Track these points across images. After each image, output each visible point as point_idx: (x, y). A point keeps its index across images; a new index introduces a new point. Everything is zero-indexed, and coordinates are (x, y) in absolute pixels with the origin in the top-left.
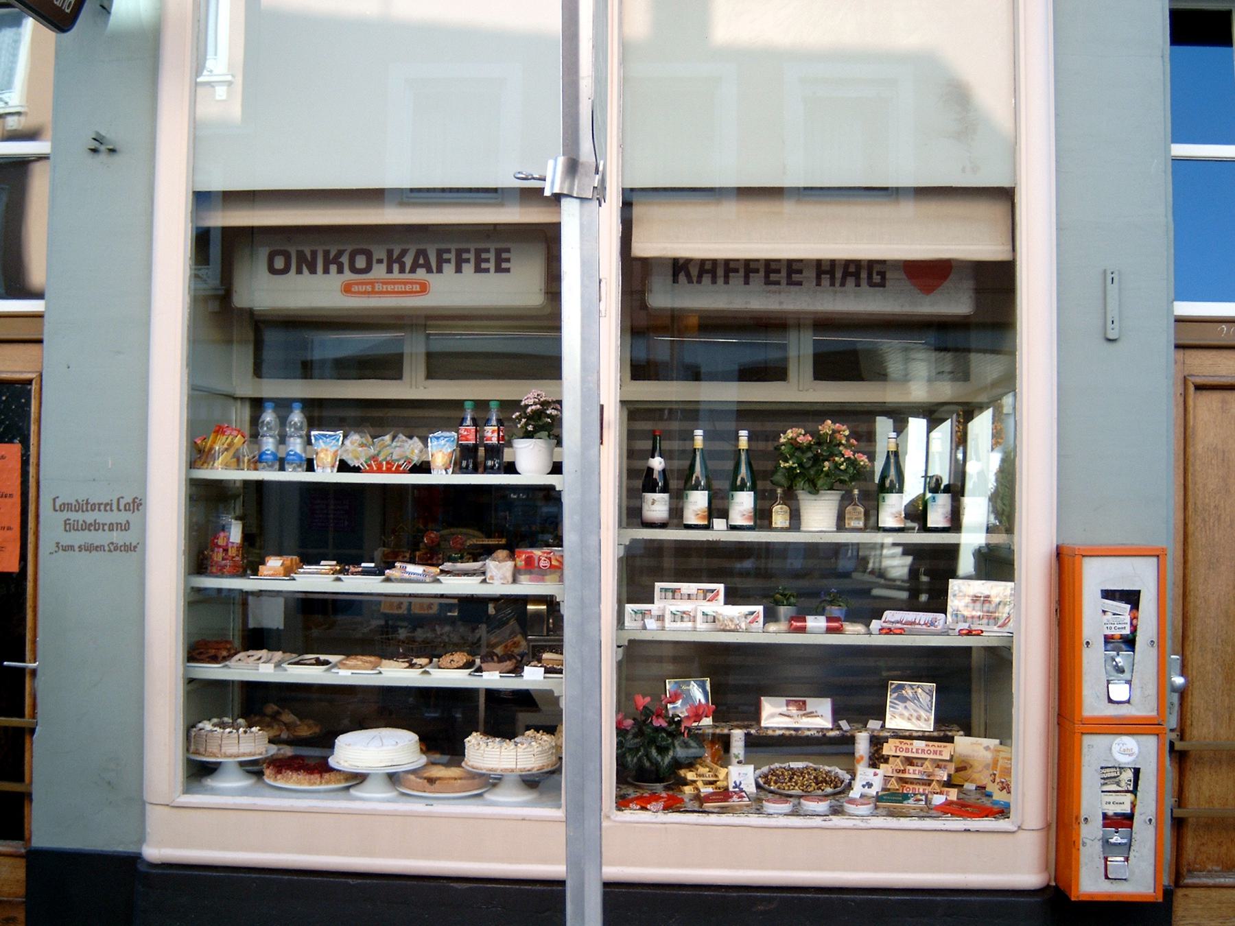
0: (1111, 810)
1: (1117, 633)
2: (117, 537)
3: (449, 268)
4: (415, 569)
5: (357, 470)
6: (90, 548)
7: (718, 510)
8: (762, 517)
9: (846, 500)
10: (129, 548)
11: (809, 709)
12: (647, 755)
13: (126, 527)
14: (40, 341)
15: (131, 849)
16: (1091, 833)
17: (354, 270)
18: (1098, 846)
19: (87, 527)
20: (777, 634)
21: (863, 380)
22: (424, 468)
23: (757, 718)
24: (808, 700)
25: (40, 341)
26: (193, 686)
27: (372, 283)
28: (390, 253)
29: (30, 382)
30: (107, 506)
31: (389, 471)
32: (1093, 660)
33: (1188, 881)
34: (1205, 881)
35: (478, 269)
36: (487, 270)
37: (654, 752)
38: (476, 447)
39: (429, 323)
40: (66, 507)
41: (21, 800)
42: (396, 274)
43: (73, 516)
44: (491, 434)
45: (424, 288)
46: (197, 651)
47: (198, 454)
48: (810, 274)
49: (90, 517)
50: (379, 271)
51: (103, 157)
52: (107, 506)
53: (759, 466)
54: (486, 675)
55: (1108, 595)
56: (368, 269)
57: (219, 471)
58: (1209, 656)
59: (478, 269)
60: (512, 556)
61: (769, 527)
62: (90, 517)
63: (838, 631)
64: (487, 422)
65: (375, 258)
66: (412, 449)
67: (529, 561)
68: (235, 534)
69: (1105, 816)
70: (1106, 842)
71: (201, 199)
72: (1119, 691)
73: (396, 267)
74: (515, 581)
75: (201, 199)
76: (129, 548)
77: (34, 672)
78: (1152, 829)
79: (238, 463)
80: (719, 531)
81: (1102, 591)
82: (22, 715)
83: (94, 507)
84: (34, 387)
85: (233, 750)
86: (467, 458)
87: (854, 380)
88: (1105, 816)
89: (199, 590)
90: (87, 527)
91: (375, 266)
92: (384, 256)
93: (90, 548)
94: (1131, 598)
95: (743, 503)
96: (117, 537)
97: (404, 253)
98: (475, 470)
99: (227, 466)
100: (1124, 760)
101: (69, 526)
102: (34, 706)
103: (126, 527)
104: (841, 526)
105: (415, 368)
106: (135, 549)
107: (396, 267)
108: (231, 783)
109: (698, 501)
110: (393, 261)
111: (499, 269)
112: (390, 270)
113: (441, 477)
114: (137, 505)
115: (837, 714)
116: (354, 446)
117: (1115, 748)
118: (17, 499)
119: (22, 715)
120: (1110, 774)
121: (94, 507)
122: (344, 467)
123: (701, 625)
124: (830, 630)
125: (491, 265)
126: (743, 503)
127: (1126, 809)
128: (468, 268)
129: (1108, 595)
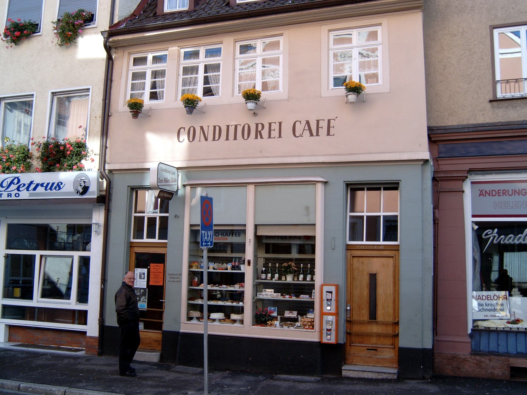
0: (328, 328)
1: (329, 298)
2: (178, 280)
3: (231, 236)
4: (225, 286)
5: (216, 269)
6: (173, 281)
7: (272, 277)
8: (280, 278)
9: (295, 276)
10: (179, 282)
11: (293, 313)
12: (261, 318)
13: (179, 278)
14: (167, 247)
15: (179, 331)
16: (325, 331)
17: (216, 236)
18: (326, 334)
19: (173, 278)
20: (281, 298)
21: (306, 254)
22: (227, 269)
23: (283, 315)
24: (293, 311)
25: (167, 247)
26: (189, 305)
27: (219, 238)
28: (222, 233)
29: (165, 254)
30: (176, 275)
31: (221, 270)
32: (325, 302)
33: (352, 345)
34: (355, 345)
35: (235, 236)
36: (501, 195)
37: (261, 318)
38: (234, 266)
39: (436, 224)
40: (170, 275)
41: (162, 323)
42: (223, 237)
43: (171, 276)
44: (237, 264)
45: (227, 239)
46: (189, 299)
47: (190, 266)
48: (280, 237)
49: (174, 276)
50: (220, 236)
51: (176, 218)
52: (176, 275)
53: (280, 269)
54: (233, 303)
55: (327, 292)
56: (218, 236)
57: (194, 269)
58: (356, 304)
59: (235, 236)
60: (239, 284)
61: (281, 280)
62: (174, 276)
63: (291, 298)
64: (236, 262)
65: (219, 234)
66: (225, 265)
67: (241, 285)
68: (196, 279)
69: (327, 329)
70: (327, 334)
71: (191, 226)
72: (329, 308)
73: (223, 235)
74: (240, 288)
75: (191, 226)
76: (179, 282)
77: (164, 302)
78: (323, 328)
79: (197, 267)
80: (274, 281)
81: (79, 256)
82: (162, 309)
83: (174, 275)
84: (166, 255)
85: (195, 315)
86: (233, 268)
87: (465, 251)
88: (327, 329)
89: (190, 289)
90: (173, 278)
91: (219, 235)
92: (221, 234)
93: (173, 281)
94: (331, 292)
95: (277, 276)
96: (178, 280)
97: (224, 233)
98: (234, 270)
99: (195, 268)
100: (330, 320)
101: (171, 278)
102: (164, 308)
103: (179, 278)
104: (294, 280)
105: (294, 250)
106: (180, 282)
107: (223, 235)
108: (194, 321)
109: (269, 275)
110: (222, 234)
111: (239, 236)
112: (222, 236)
113: (229, 271)
114: (181, 274)
115: (298, 314)
116: (216, 265)
117: (328, 318)
118: (163, 273)
119: (162, 309)
120: (328, 322)
121: (174, 275)
122: (214, 269)
123: (269, 296)
124: (289, 298)
125: (237, 235)
126: (277, 276)
127: (331, 328)
128: (234, 236)
129: (327, 292)
